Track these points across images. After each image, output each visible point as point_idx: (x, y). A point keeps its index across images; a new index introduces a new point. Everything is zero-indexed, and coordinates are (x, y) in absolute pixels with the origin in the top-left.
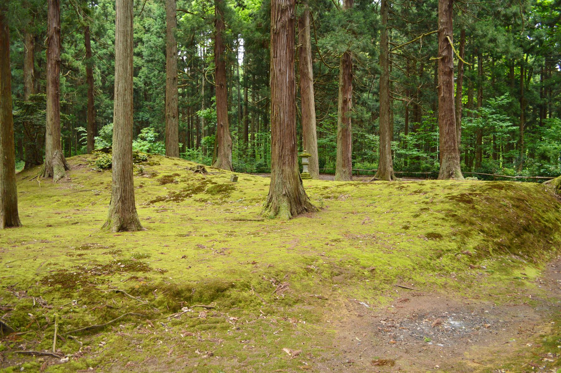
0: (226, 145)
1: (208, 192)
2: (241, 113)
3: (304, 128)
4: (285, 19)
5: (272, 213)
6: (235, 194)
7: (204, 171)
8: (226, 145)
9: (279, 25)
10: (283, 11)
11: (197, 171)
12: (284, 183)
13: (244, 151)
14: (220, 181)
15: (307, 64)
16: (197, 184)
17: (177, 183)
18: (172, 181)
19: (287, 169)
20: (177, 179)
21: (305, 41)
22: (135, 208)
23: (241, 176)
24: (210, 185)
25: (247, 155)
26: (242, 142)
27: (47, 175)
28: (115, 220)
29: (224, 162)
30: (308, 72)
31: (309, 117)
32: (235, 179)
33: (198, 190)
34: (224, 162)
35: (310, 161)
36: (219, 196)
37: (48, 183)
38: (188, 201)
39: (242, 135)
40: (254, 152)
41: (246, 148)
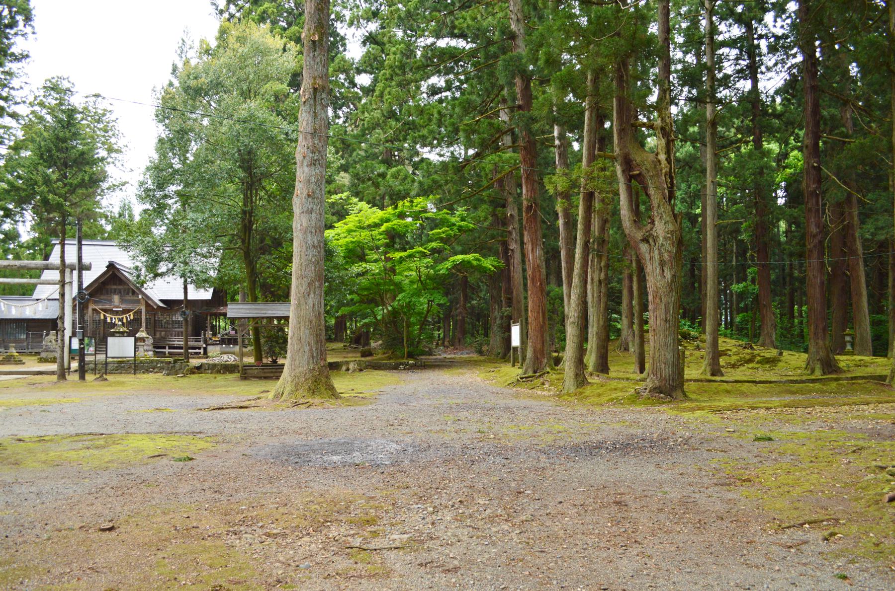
0: (769, 324)
1: (758, 362)
2: (784, 279)
3: (854, 306)
4: (816, 241)
5: (809, 372)
6: (780, 364)
7: (752, 348)
8: (769, 324)
9: (812, 245)
10: (814, 236)
11: (745, 348)
12: (818, 352)
13: (789, 330)
14: (768, 355)
15: (855, 241)
16: (748, 357)
17: (730, 356)
18: (726, 355)
19: (821, 342)
20: (729, 353)
21: (853, 218)
22: (851, 305)
23: (785, 353)
24: (759, 358)
25: (792, 335)
26: (785, 319)
27: (623, 349)
28: (708, 369)
29: (768, 341)
30: (857, 249)
31: (860, 295)
32: (781, 354)
33: (750, 361)
34: (768, 341)
35: (853, 338)
36: (767, 366)
37: (626, 354)
38: (742, 368)
39: (786, 310)
40: (802, 331)
41: (791, 327)
